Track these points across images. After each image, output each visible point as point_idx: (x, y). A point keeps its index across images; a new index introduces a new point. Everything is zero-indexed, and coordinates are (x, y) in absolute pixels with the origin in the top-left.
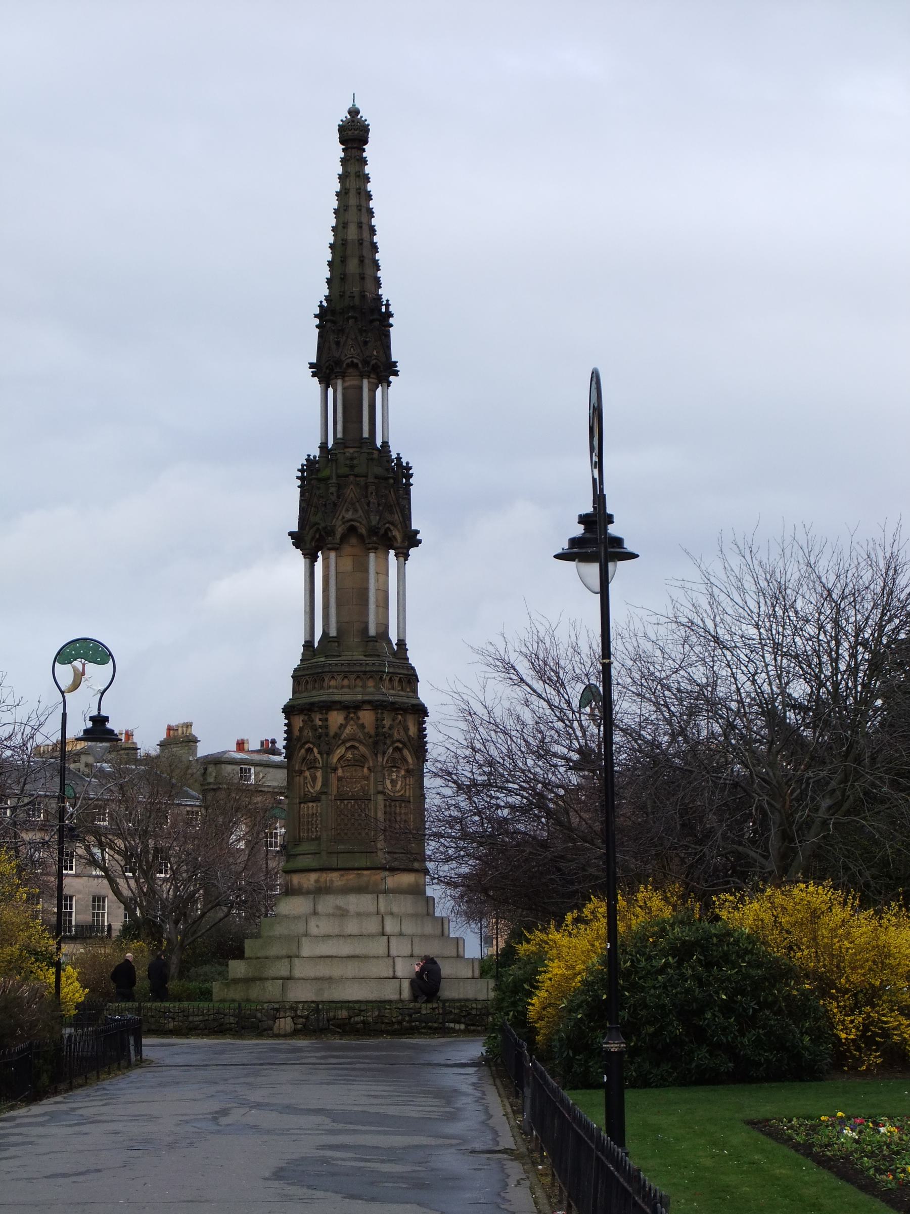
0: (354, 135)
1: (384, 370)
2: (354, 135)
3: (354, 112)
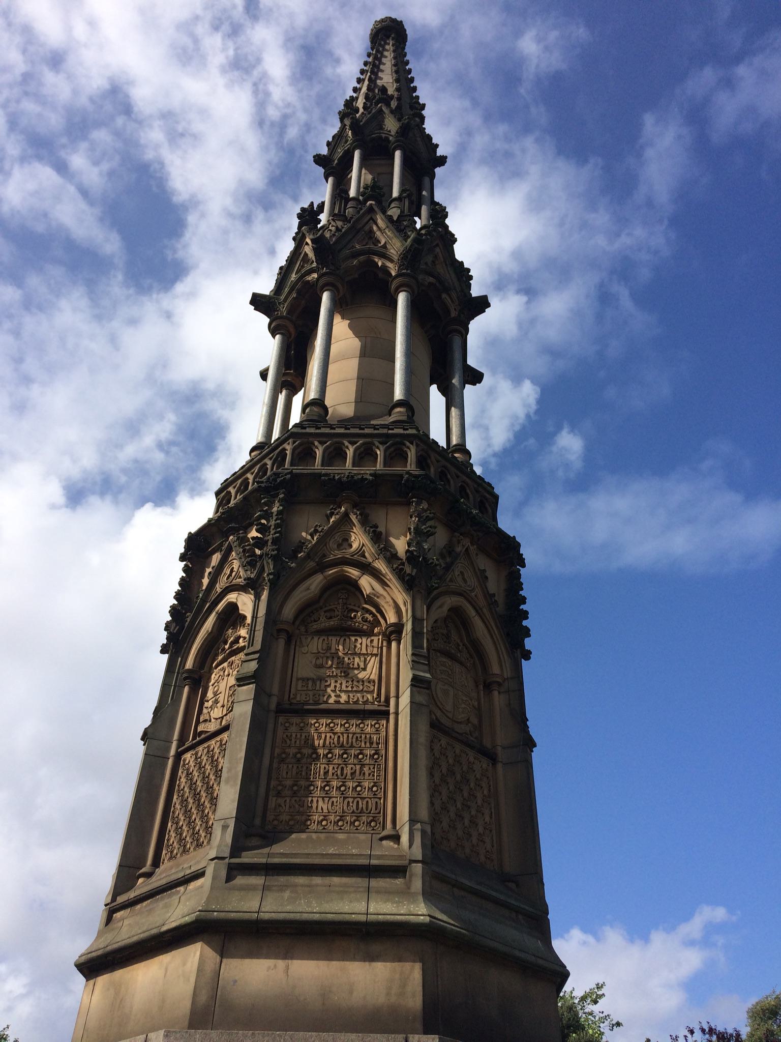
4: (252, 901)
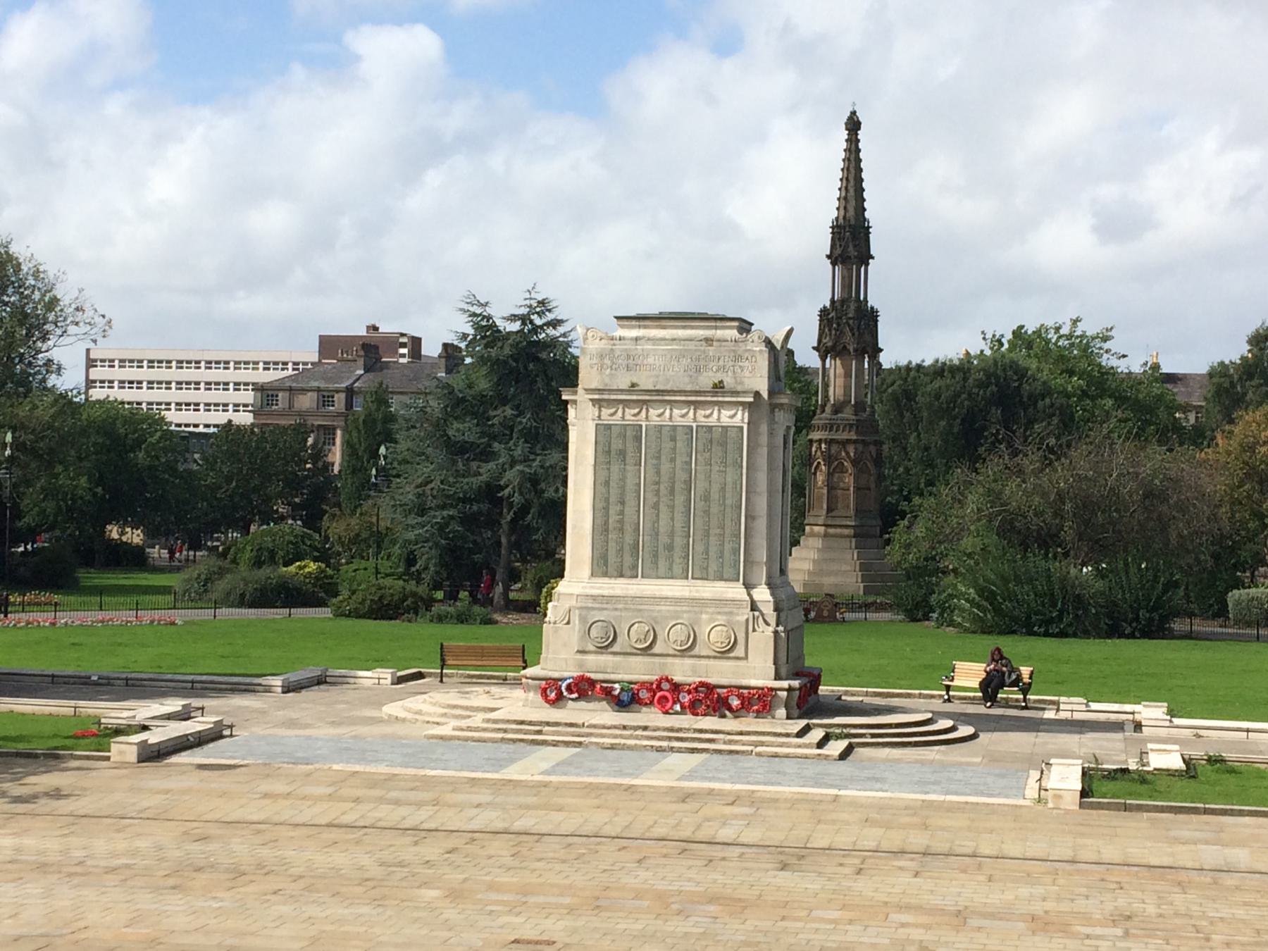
0: (853, 125)
1: (865, 257)
2: (853, 125)
3: (854, 113)
4: (829, 523)
